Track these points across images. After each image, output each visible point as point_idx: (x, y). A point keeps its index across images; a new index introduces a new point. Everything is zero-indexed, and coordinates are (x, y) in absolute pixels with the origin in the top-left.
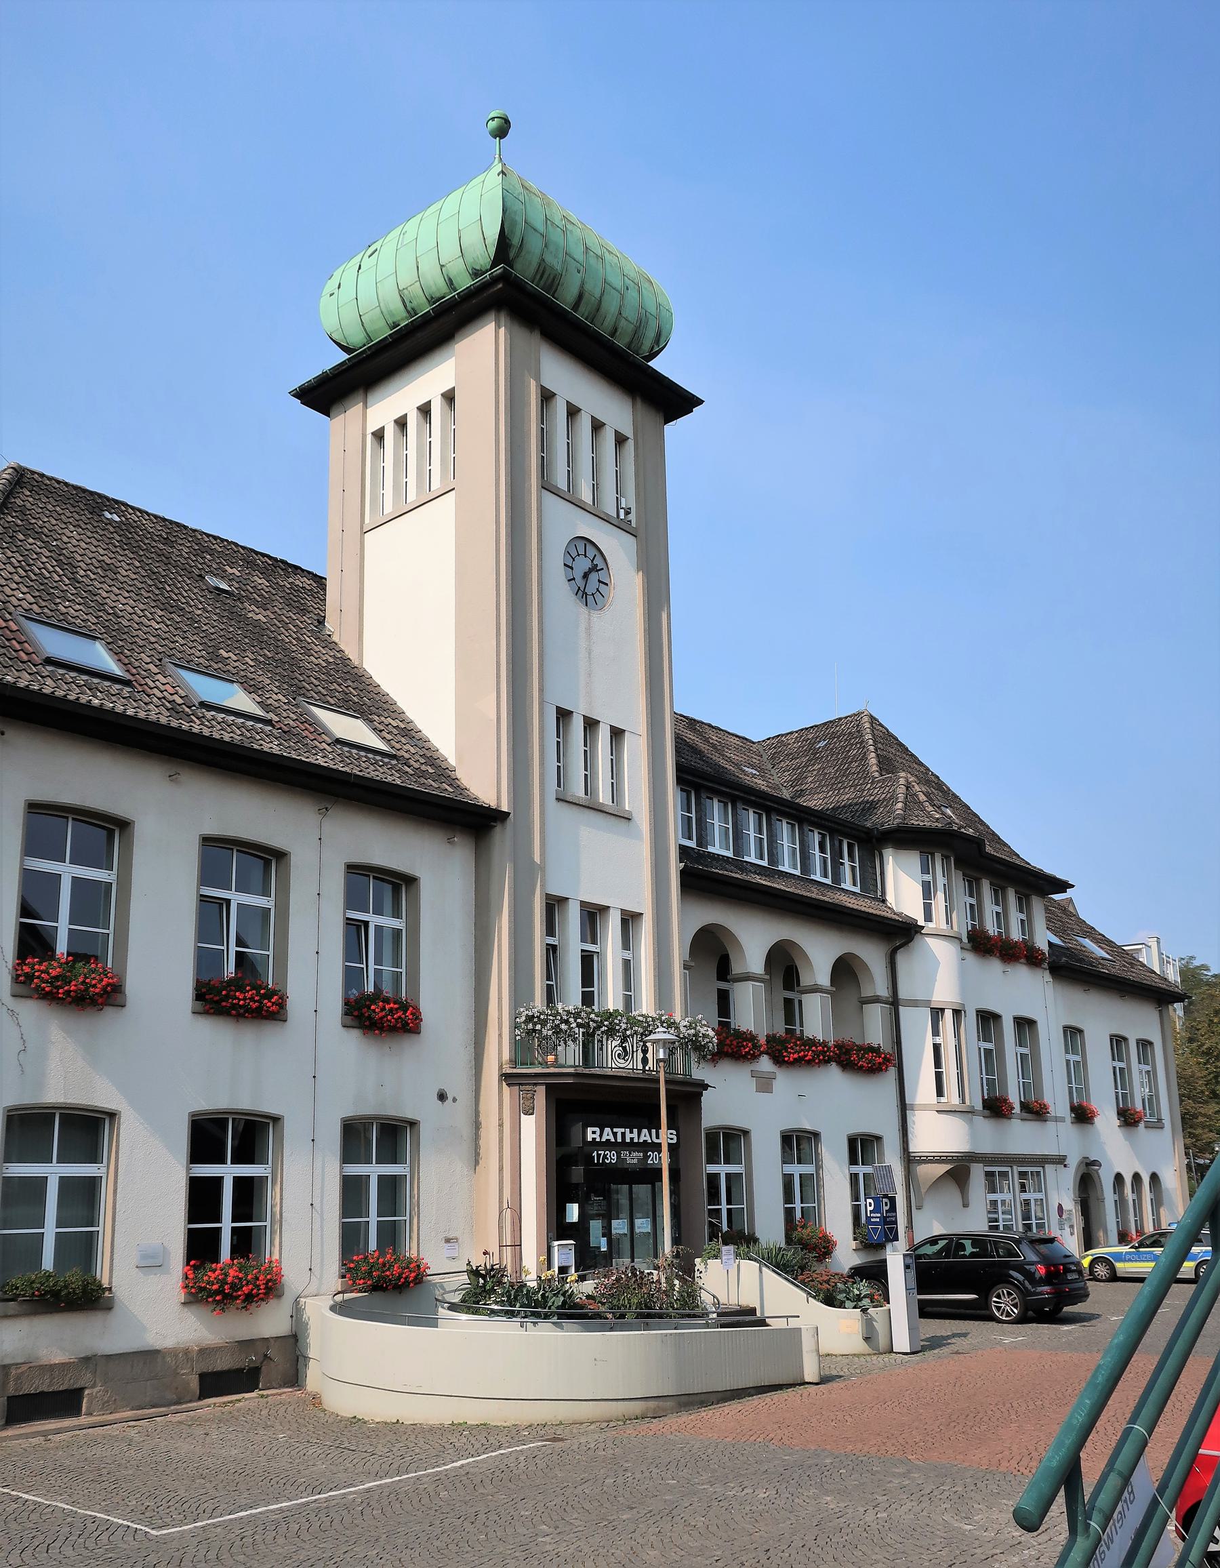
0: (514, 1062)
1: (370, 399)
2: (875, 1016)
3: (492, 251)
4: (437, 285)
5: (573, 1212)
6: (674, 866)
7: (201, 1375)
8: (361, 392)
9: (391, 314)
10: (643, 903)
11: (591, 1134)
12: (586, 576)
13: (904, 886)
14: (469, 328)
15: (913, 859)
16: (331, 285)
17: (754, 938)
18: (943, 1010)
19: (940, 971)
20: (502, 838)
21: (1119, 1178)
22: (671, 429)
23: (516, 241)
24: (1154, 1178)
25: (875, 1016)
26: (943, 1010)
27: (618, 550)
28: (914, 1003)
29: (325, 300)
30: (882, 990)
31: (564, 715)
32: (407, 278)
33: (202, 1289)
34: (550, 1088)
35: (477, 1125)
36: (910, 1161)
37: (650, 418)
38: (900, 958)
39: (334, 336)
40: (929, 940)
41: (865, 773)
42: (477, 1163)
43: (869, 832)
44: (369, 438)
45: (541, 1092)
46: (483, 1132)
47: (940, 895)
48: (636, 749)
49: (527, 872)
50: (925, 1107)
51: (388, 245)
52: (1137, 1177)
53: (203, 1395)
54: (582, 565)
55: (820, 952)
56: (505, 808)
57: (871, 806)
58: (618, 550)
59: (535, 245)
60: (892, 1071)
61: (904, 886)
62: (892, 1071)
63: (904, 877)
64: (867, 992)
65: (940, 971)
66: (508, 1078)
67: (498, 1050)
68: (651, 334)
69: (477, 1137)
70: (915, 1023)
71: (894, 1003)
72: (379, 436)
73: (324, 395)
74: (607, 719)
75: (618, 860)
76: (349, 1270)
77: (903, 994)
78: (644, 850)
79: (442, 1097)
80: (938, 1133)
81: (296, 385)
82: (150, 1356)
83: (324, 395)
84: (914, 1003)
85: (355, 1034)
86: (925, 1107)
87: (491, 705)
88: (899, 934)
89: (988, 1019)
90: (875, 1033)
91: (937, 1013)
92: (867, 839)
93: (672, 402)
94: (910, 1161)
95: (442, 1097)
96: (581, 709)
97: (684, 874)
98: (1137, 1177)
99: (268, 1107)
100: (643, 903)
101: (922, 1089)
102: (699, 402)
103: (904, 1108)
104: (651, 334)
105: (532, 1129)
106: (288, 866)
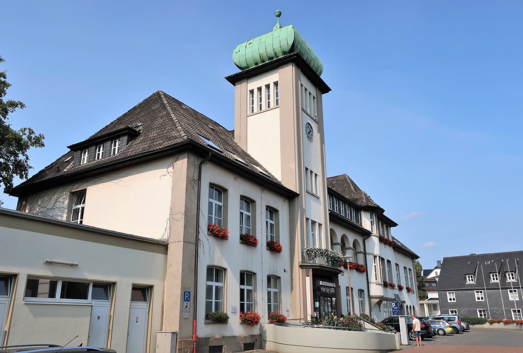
0: (302, 262)
1: (249, 81)
2: (361, 257)
3: (290, 47)
4: (271, 53)
5: (317, 304)
6: (328, 212)
7: (244, 344)
8: (246, 80)
9: (256, 60)
10: (323, 222)
11: (321, 283)
12: (309, 133)
13: (366, 222)
14: (283, 66)
15: (368, 215)
16: (236, 50)
17: (340, 232)
18: (376, 256)
19: (374, 246)
20: (297, 200)
21: (407, 306)
22: (324, 96)
23: (296, 45)
24: (413, 307)
25: (361, 257)
26: (376, 256)
27: (314, 126)
28: (370, 254)
29: (234, 54)
30: (362, 250)
31: (307, 169)
32: (262, 51)
33: (246, 319)
34: (313, 270)
35: (292, 279)
36: (370, 297)
37: (319, 92)
38: (366, 241)
39: (237, 64)
40: (373, 237)
41: (352, 191)
42: (292, 289)
43: (358, 206)
44: (248, 92)
45: (311, 270)
46: (294, 281)
47: (375, 225)
48: (320, 179)
49: (303, 211)
50: (373, 283)
51: (256, 41)
52: (410, 306)
53: (245, 350)
54: (308, 130)
55: (351, 237)
56: (298, 192)
57: (356, 200)
58: (314, 126)
59: (299, 47)
60: (365, 273)
61: (366, 222)
62: (365, 273)
63: (366, 220)
64: (358, 250)
65: (374, 246)
66: (301, 267)
67: (298, 259)
68: (319, 72)
69: (292, 283)
70: (370, 258)
71: (365, 254)
72: (252, 92)
73: (234, 80)
74: (315, 171)
75: (318, 209)
76: (270, 317)
77: (367, 252)
78: (322, 207)
79: (285, 271)
80: (376, 290)
81: (227, 75)
82: (234, 337)
83: (234, 80)
84: (370, 254)
85: (269, 252)
86: (373, 283)
87: (293, 166)
88: (366, 234)
89: (382, 259)
90: (361, 262)
91: (375, 257)
92: (358, 209)
93: (323, 88)
94: (370, 297)
95: (285, 271)
96: (310, 168)
97: (330, 214)
98: (410, 306)
99: (254, 271)
100: (323, 222)
101: (372, 279)
102: (331, 90)
103: (368, 283)
104: (319, 72)
105: (309, 280)
106: (255, 205)
